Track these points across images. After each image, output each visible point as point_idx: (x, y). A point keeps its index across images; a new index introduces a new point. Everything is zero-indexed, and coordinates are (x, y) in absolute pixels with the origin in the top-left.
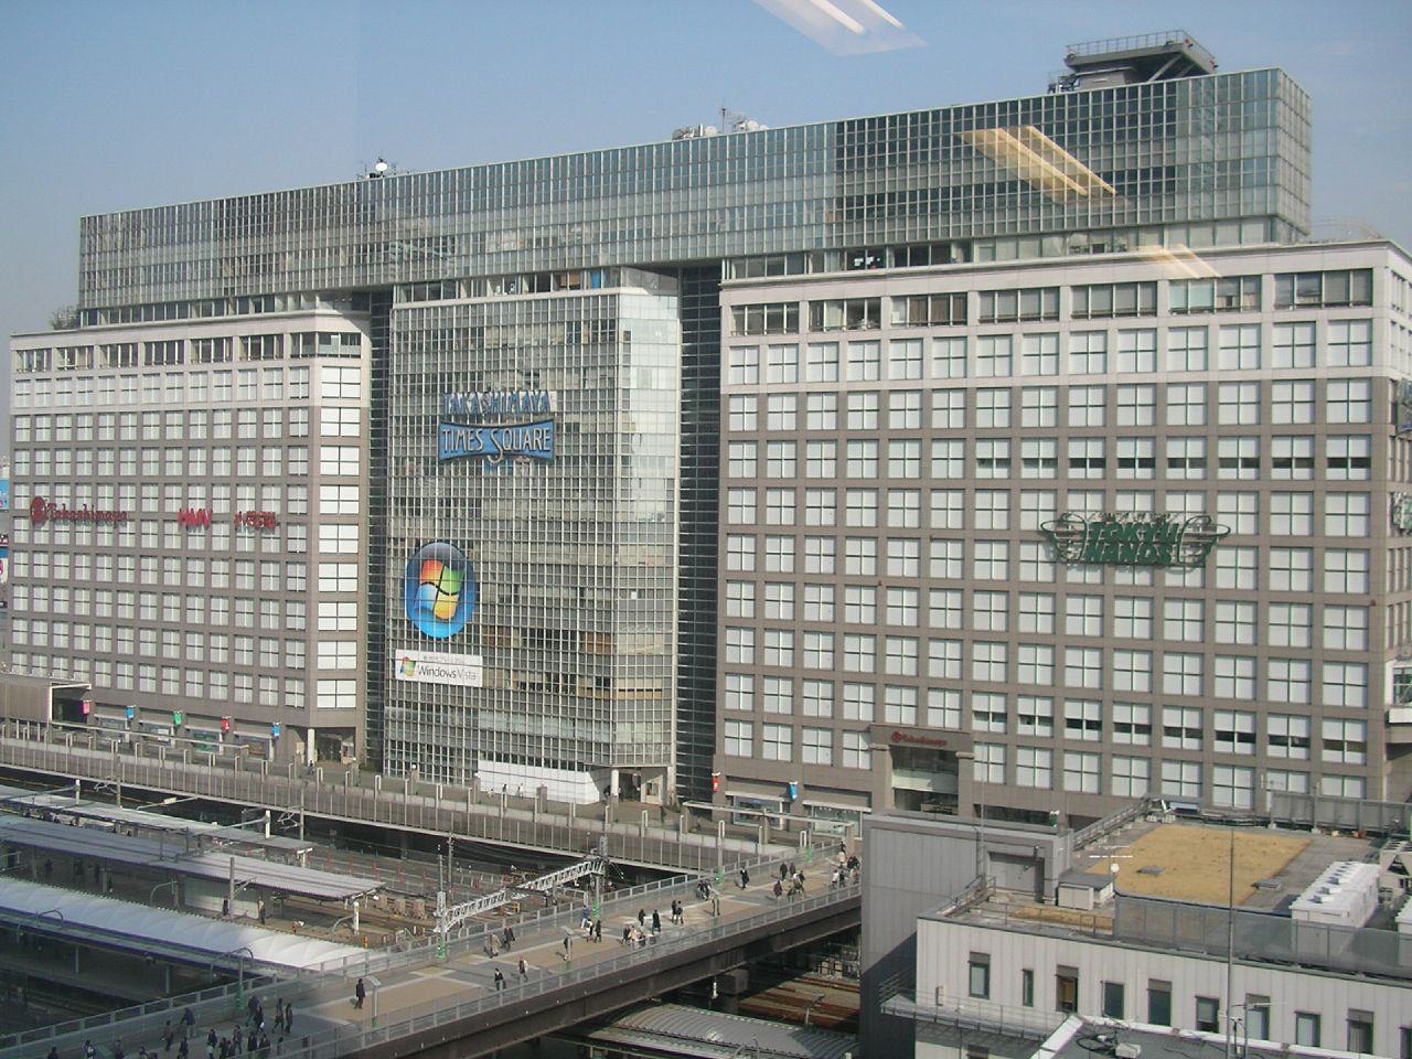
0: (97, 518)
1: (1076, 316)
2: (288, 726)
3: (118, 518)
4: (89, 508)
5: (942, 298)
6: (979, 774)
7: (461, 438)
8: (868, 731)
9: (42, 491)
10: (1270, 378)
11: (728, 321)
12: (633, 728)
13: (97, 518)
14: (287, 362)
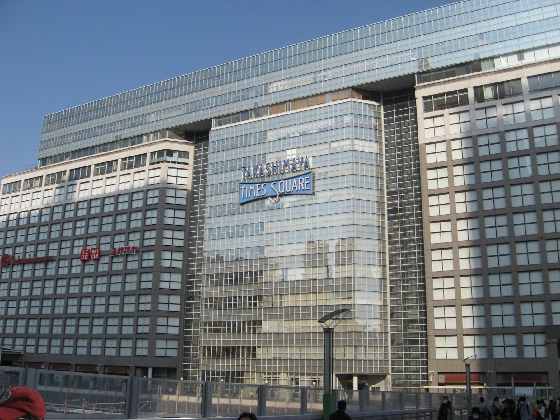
0: (35, 261)
1: (151, 164)
2: (439, 373)
3: (47, 260)
4: (32, 257)
5: (138, 157)
6: (440, 354)
7: (252, 190)
8: (542, 331)
9: (9, 252)
10: (424, 143)
11: (420, 104)
12: (355, 351)
13: (35, 261)
14: (148, 167)
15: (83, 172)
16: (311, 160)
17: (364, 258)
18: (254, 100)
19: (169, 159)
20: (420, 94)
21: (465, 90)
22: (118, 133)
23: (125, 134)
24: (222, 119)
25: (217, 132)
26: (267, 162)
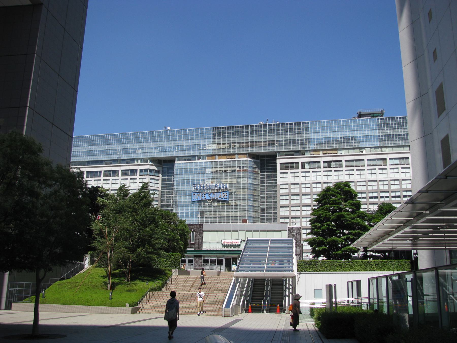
15: (98, 174)
16: (228, 185)
17: (350, 146)
18: (199, 152)
19: (150, 174)
20: (279, 161)
21: (298, 163)
22: (119, 156)
23: (124, 157)
24: (180, 158)
25: (178, 164)
26: (206, 183)
